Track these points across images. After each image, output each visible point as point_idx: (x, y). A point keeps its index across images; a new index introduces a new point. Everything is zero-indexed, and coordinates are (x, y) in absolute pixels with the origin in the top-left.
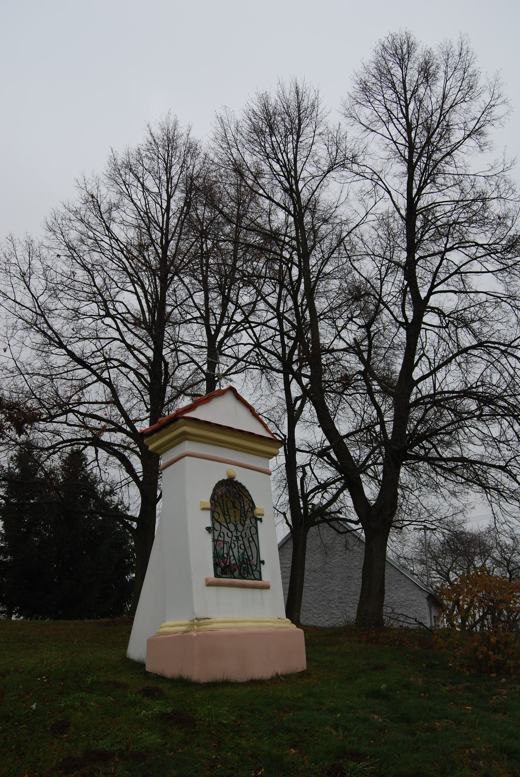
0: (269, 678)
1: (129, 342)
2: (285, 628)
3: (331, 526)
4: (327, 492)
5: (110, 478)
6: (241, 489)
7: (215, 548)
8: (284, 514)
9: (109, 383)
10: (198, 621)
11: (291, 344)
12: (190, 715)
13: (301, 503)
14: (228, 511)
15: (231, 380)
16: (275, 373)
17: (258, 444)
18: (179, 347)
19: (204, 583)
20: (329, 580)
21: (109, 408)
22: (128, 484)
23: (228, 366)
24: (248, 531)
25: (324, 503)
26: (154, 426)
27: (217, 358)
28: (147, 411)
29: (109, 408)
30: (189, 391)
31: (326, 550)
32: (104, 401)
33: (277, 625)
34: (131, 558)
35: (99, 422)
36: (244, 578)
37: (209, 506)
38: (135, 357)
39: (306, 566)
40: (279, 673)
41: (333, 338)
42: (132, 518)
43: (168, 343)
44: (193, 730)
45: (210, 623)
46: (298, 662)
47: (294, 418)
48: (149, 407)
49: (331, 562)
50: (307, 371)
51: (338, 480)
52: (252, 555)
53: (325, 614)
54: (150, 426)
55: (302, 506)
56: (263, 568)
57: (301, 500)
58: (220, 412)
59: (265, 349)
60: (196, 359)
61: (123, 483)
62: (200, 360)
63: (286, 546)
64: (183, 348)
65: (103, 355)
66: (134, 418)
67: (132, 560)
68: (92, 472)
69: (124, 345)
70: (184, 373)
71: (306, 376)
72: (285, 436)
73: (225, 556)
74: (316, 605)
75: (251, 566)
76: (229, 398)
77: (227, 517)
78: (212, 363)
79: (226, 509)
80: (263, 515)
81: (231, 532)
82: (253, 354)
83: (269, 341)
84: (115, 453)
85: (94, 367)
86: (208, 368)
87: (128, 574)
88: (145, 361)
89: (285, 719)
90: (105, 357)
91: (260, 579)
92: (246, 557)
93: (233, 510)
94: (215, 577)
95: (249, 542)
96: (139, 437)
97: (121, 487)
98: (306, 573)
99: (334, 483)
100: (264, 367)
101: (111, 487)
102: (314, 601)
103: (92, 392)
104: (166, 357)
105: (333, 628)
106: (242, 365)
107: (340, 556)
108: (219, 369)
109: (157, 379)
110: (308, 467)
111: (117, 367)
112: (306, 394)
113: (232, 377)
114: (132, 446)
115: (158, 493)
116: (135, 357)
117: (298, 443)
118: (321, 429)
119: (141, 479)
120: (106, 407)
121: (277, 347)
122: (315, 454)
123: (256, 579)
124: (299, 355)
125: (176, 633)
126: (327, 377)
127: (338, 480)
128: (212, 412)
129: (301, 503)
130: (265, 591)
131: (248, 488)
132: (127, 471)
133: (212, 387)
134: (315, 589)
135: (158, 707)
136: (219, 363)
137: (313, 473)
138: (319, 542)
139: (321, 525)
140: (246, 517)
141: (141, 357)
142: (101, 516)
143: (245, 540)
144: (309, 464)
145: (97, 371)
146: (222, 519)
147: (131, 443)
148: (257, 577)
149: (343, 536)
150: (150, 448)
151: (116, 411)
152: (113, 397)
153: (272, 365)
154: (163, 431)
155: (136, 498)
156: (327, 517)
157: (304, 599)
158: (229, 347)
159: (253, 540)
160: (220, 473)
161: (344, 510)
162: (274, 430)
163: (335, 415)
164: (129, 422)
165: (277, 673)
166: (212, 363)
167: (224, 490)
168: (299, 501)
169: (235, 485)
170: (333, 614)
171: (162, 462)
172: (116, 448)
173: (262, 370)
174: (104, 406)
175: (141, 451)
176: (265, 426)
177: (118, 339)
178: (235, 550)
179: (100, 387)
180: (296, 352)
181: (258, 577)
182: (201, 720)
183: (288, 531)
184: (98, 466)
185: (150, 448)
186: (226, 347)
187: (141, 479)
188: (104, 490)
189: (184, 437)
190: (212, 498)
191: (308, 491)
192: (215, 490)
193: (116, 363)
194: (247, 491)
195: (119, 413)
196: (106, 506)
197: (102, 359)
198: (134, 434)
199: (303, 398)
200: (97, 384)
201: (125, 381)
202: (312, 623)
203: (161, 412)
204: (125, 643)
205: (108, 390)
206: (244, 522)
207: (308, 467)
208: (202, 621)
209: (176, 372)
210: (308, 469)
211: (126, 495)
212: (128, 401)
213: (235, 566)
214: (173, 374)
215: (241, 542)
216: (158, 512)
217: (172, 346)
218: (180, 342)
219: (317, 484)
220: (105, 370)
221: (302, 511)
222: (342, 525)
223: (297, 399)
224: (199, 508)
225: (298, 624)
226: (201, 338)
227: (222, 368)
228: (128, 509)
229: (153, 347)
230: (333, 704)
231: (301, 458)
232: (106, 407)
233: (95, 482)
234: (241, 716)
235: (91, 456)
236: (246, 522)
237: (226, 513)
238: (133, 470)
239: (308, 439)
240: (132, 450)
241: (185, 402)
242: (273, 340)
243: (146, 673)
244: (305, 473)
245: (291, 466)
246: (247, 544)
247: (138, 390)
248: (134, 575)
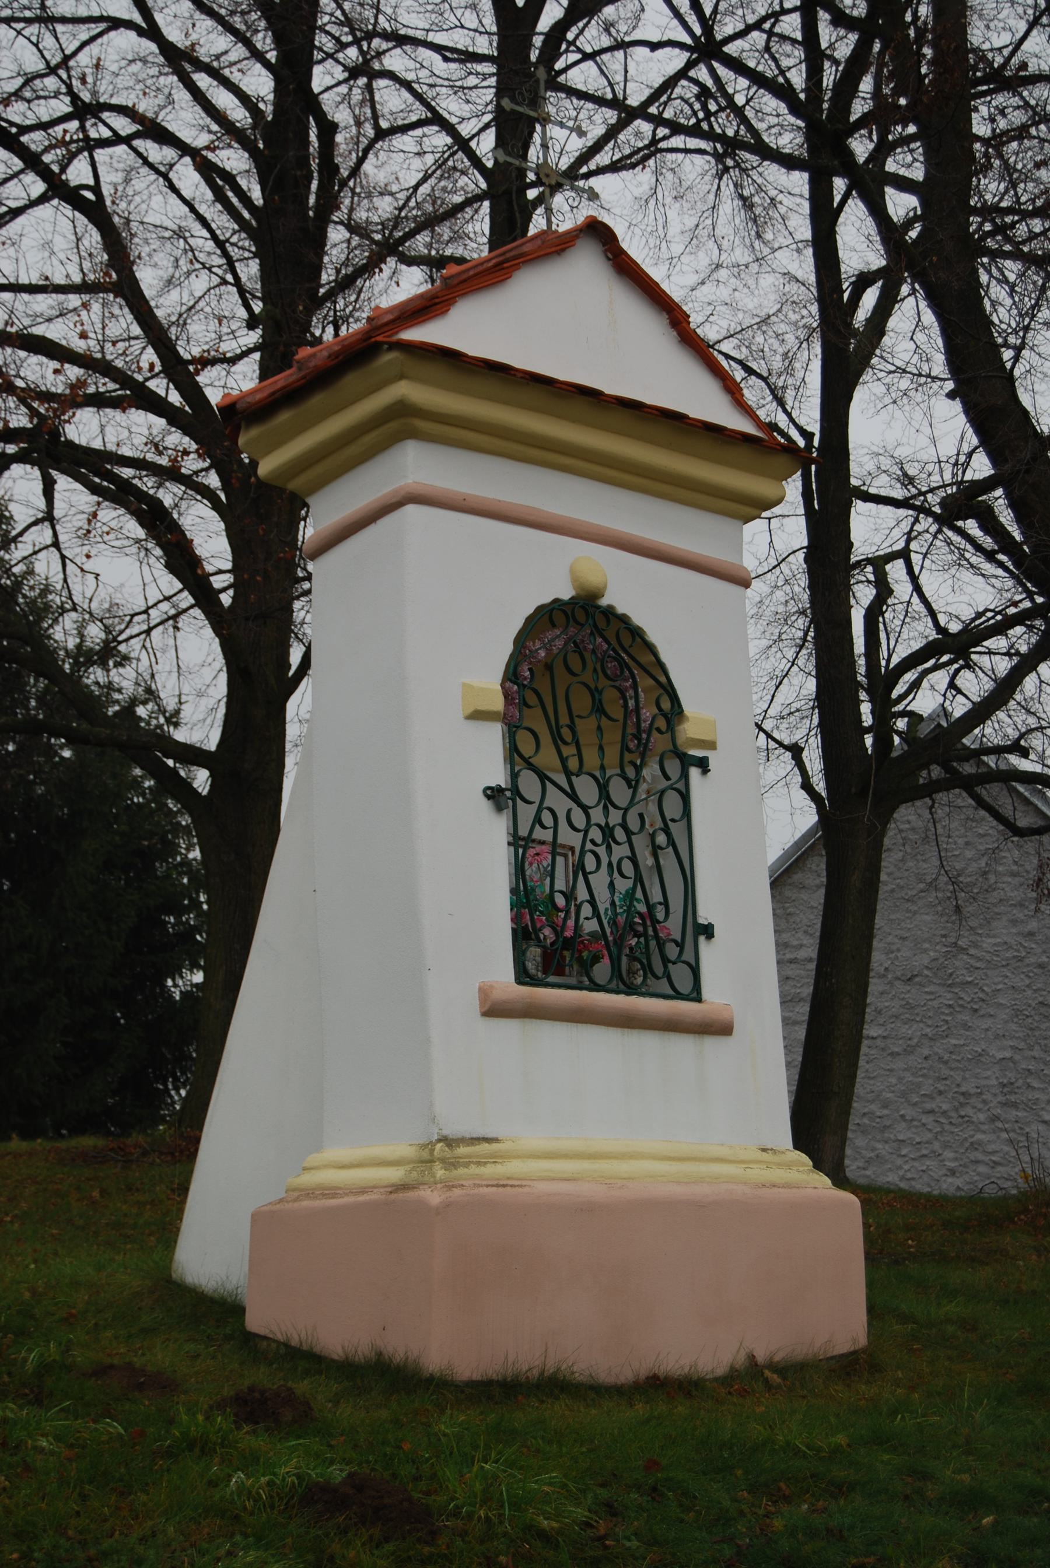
0: (720, 1371)
1: (174, 35)
2: (787, 1186)
3: (981, 803)
4: (969, 666)
5: (102, 593)
6: (627, 641)
7: (519, 869)
8: (796, 751)
9: (93, 208)
10: (449, 1148)
11: (844, 50)
12: (416, 1495)
13: (866, 708)
14: (572, 728)
15: (593, 196)
16: (773, 172)
17: (704, 459)
18: (379, 54)
19: (474, 1005)
20: (965, 1017)
21: (96, 307)
22: (175, 617)
23: (581, 133)
24: (653, 807)
25: (957, 713)
26: (281, 380)
27: (536, 101)
28: (252, 323)
29: (96, 307)
30: (420, 243)
31: (958, 899)
32: (77, 279)
33: (758, 1173)
34: (187, 910)
35: (55, 364)
36: (631, 990)
37: (498, 703)
38: (199, 96)
39: (878, 958)
40: (761, 1357)
41: (1023, 26)
42: (193, 755)
43: (337, 40)
44: (426, 1550)
45: (496, 1158)
46: (836, 1314)
47: (846, 355)
48: (257, 307)
49: (975, 945)
50: (909, 163)
51: (1019, 619)
52: (666, 903)
53: (946, 1146)
54: (262, 378)
55: (867, 720)
56: (709, 954)
57: (863, 695)
58: (544, 323)
59: (737, 66)
60: (451, 106)
61: (155, 615)
62: (466, 110)
63: (797, 877)
64: (396, 61)
65: (71, 92)
66: (196, 351)
67: (191, 918)
68: (30, 572)
69: (153, 47)
70: (397, 170)
71: (904, 184)
72: (807, 436)
73: (560, 901)
74: (909, 1112)
75: (661, 946)
76: (585, 267)
77: (568, 751)
78: (515, 126)
79: (564, 720)
80: (712, 745)
81: (585, 809)
82: (685, 89)
83: (755, 34)
84: (123, 495)
85: (34, 141)
86: (500, 142)
87: (175, 971)
88: (239, 115)
89: (778, 1523)
90: (75, 98)
91: (696, 995)
92: (642, 908)
93: (592, 722)
94: (519, 981)
95: (655, 850)
96: (215, 429)
97: (148, 632)
98: (875, 986)
99: (1001, 629)
100: (732, 145)
101: (107, 630)
102: (904, 1094)
103: (26, 242)
104: (328, 101)
105: (973, 1200)
106: (638, 134)
107: (1014, 922)
108: (545, 146)
109: (289, 193)
110: (900, 563)
111: (127, 140)
112: (907, 259)
113: (594, 182)
114: (191, 464)
115: (295, 657)
116: (199, 96)
117: (860, 467)
118: (957, 406)
119: (226, 599)
120: (85, 306)
121: (785, 63)
122: (928, 512)
123: (678, 996)
124: (877, 93)
125: (363, 1190)
126: (991, 188)
127: (1019, 619)
128: (516, 325)
129: (866, 708)
130: (711, 1043)
131: (653, 636)
132: (171, 567)
133: (514, 218)
134: (909, 1051)
135: (291, 1462)
136: (545, 120)
137: (918, 589)
138: (930, 867)
139: (942, 797)
140: (644, 751)
141: (224, 99)
142: (70, 743)
143: (641, 843)
144: (904, 554)
145: (47, 158)
146: (547, 757)
147: (186, 453)
148: (684, 985)
149: (1030, 844)
150: (265, 468)
151: (125, 323)
152: (111, 264)
153: (766, 138)
154: (317, 401)
155: (208, 674)
156: (968, 768)
157: (862, 1087)
158: (586, 57)
159: (671, 842)
160: (548, 573)
161: (1036, 741)
162: (769, 412)
163: (1018, 350)
164: (178, 369)
165: (752, 1358)
166: (515, 126)
167: (559, 643)
168: (858, 702)
169: (601, 623)
170: (974, 1146)
171: (308, 532)
172: (127, 472)
173: (719, 158)
174: (74, 300)
175: (224, 489)
176: (732, 390)
177: (129, 25)
178: (600, 881)
179: (56, 221)
180: (866, 85)
181: (685, 987)
182: (456, 1514)
183: (807, 817)
184: (56, 544)
185: (265, 468)
186: (574, 57)
187: (226, 599)
188: (79, 647)
189: (400, 424)
190: (512, 674)
191: (895, 660)
192: (521, 640)
193: (124, 126)
194: (651, 649)
195: (136, 330)
196: (88, 705)
197: (62, 106)
198: (198, 419)
199: (889, 282)
200: (44, 211)
201: (157, 201)
202: (891, 1178)
203: (307, 327)
204: (168, 1230)
205: (93, 238)
206: (638, 769)
207: (900, 563)
208: (463, 1150)
209: (368, 167)
210: (896, 571)
211: (165, 665)
212: (169, 283)
213: (597, 943)
214: (355, 171)
215: (621, 851)
216: (292, 731)
217: (352, 52)
218: (386, 36)
219: (933, 635)
220: (80, 151)
221: (869, 740)
222: (1027, 802)
223: (864, 281)
224: (458, 712)
225: (840, 1180)
226: (470, 19)
227: (559, 143)
228: (174, 719)
229: (272, 56)
230: (966, 1477)
231: (870, 529)
232: (85, 306)
233: (43, 610)
234: (609, 1505)
235: (28, 504)
236: (645, 772)
237: (566, 733)
238: (196, 562)
239: (901, 452)
240: (188, 481)
241: (401, 284)
242: (770, 33)
243: (250, 1340)
244: (883, 590)
245: (828, 555)
246: (646, 860)
247: (214, 237)
248: (198, 977)
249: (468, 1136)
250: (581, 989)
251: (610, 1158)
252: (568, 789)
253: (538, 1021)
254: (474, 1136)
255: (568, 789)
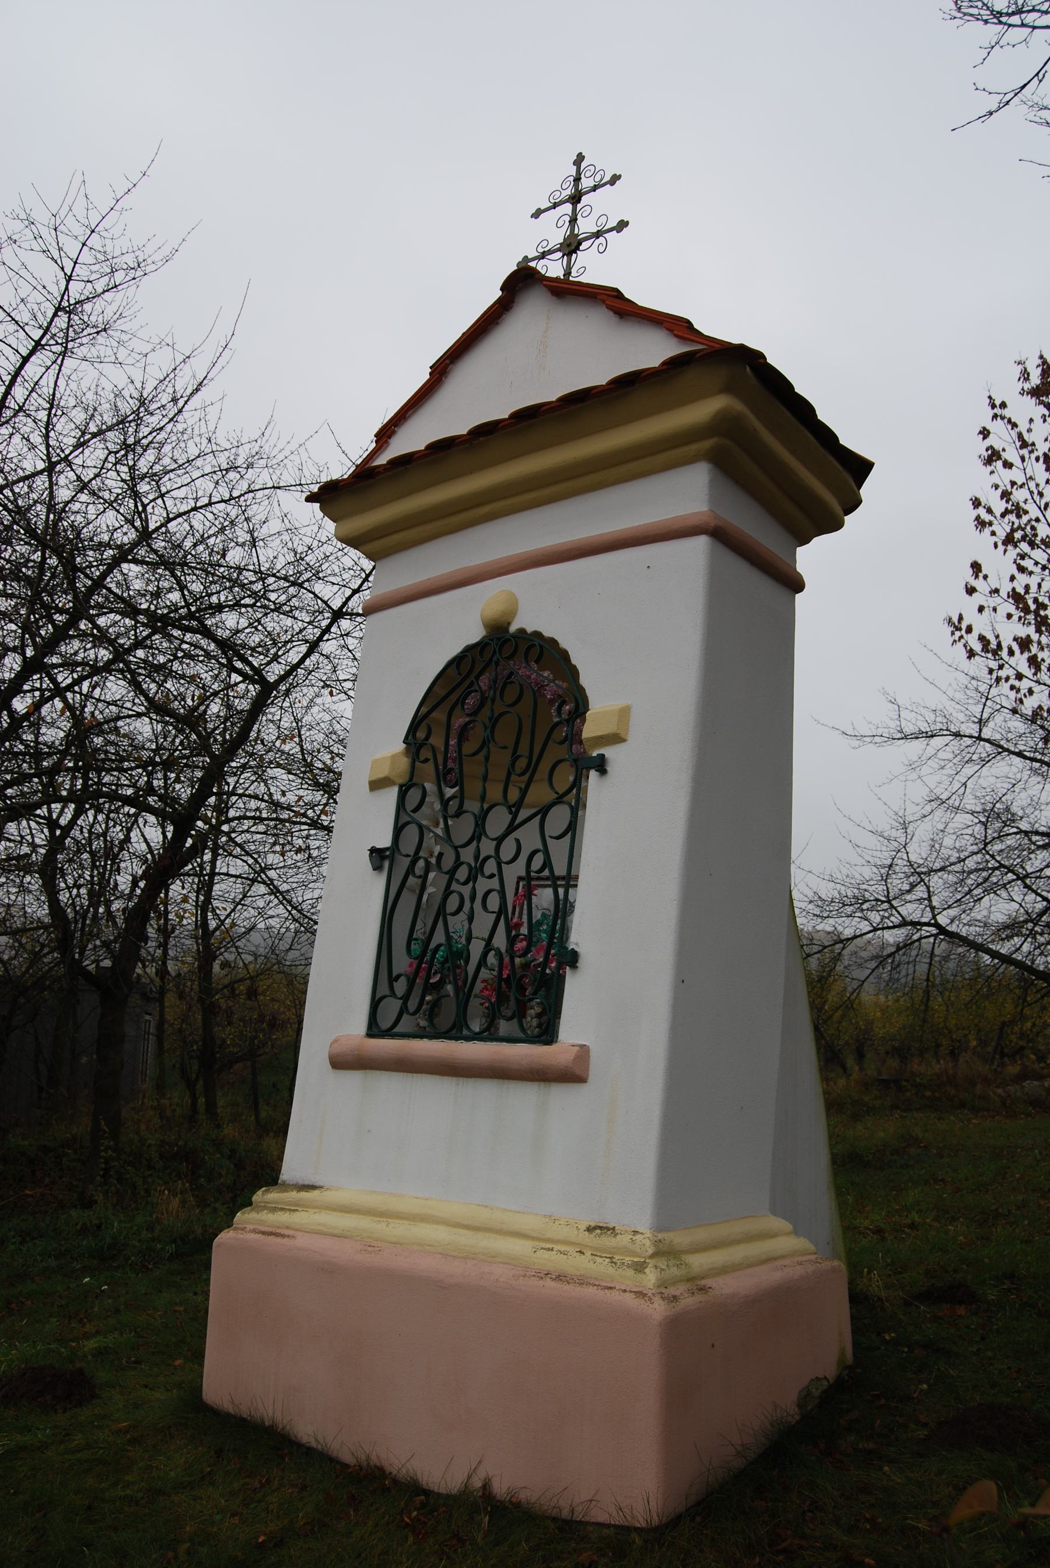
2: (582, 1281)
56: (576, 990)
130: (560, 1095)
165: (486, 1486)
249: (301, 1183)
250: (421, 1037)
251: (402, 1218)
252: (517, 822)
253: (378, 1072)
254: (306, 1183)
255: (517, 822)
